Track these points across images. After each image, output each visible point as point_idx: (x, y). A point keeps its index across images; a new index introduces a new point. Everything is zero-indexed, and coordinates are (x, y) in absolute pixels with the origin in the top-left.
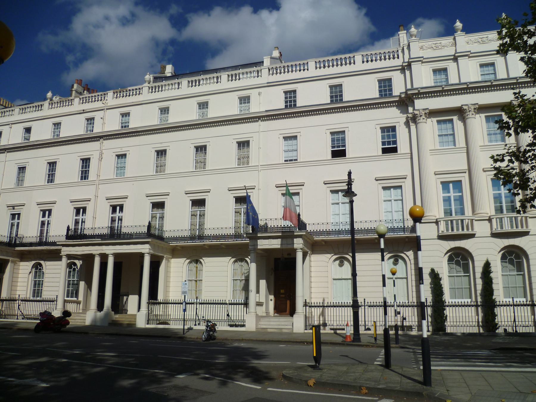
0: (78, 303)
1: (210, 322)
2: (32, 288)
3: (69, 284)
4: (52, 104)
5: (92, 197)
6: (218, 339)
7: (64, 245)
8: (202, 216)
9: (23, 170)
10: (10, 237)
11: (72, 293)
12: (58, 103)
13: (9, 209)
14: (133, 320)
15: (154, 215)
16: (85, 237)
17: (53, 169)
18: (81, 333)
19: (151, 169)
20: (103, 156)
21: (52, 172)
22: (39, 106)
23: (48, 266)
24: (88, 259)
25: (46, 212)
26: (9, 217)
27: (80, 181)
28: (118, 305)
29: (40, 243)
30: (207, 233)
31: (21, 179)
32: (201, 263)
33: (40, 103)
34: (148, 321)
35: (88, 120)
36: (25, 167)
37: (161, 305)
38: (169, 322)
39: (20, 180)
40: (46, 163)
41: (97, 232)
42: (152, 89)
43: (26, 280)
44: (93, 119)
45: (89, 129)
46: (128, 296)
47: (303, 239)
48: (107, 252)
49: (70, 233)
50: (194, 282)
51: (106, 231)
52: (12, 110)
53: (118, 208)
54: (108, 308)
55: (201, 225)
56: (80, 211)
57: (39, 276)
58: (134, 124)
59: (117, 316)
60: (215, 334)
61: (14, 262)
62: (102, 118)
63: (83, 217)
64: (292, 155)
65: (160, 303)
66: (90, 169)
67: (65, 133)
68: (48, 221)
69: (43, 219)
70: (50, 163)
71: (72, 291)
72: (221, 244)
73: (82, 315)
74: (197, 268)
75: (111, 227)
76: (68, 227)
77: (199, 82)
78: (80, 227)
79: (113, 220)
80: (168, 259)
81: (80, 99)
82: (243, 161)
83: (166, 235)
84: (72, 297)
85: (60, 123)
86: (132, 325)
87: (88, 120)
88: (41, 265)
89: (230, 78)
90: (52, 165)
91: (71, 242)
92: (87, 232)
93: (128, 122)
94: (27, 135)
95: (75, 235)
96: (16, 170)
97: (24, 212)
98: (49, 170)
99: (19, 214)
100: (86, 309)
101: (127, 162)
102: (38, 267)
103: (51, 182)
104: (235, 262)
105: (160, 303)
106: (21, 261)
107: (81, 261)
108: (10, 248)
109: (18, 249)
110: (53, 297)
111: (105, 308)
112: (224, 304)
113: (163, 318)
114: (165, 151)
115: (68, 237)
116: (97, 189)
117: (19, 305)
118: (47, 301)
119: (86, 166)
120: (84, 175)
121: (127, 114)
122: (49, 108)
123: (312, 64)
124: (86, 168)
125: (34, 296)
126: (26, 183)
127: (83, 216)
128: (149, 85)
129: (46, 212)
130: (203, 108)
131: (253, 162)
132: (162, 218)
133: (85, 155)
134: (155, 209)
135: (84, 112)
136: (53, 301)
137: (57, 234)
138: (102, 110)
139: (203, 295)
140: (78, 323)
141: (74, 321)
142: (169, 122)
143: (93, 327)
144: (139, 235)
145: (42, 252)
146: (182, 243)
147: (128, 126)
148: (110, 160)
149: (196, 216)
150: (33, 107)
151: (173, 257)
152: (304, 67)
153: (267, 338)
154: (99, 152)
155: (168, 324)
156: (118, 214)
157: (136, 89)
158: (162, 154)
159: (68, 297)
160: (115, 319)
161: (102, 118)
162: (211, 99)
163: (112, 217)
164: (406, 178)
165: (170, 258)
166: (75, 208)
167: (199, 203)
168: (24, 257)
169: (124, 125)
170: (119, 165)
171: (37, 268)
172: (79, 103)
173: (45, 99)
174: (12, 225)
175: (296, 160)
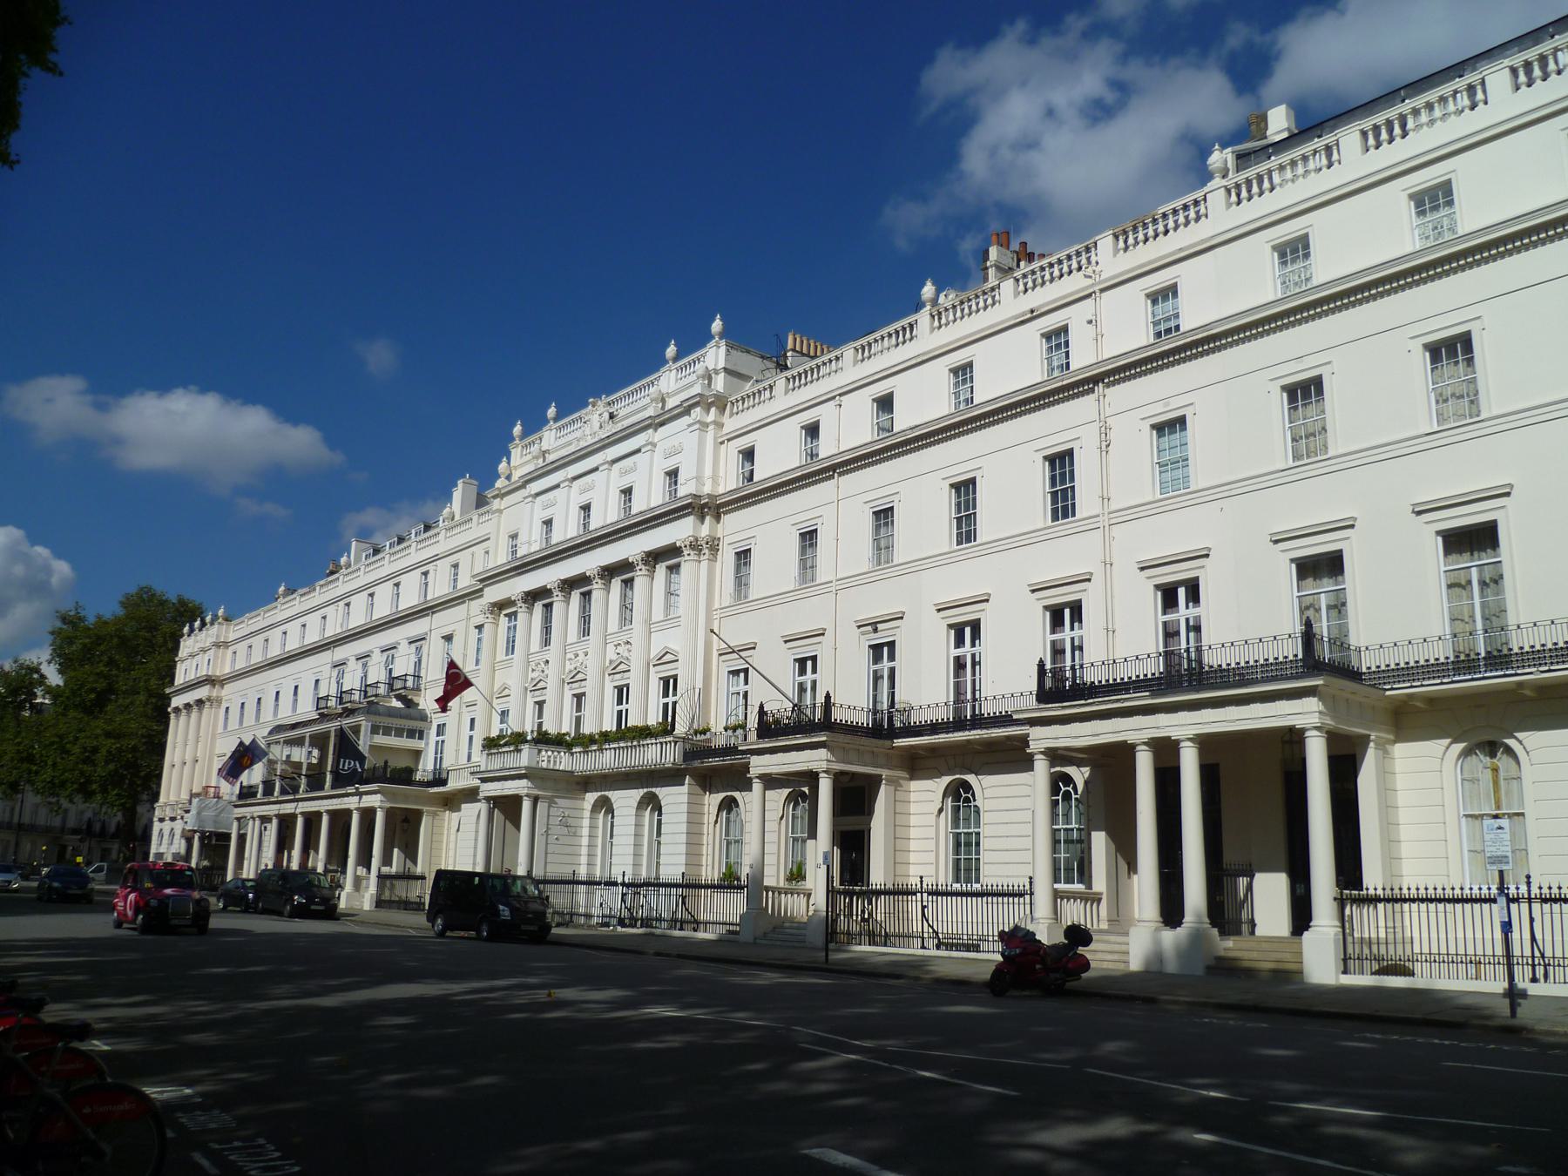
2: (951, 857)
4: (940, 314)
5: (1095, 568)
7: (1033, 722)
8: (1494, 582)
10: (875, 712)
11: (1069, 870)
12: (954, 307)
13: (863, 634)
14: (1288, 957)
16: (1092, 691)
18: (1131, 999)
19: (1278, 452)
20: (1112, 435)
21: (967, 509)
22: (904, 329)
23: (990, 789)
24: (1113, 763)
25: (966, 631)
26: (865, 655)
27: (1049, 523)
28: (1227, 911)
29: (959, 724)
30: (1520, 641)
31: (883, 545)
32: (1509, 751)
33: (905, 322)
34: (1345, 960)
35: (1048, 336)
36: (892, 508)
37: (1381, 906)
39: (882, 548)
41: (1125, 673)
42: (1238, 194)
44: (1064, 329)
45: (1055, 364)
46: (1252, 877)
48: (1174, 734)
51: (1154, 668)
52: (837, 359)
53: (1182, 592)
54: (1199, 916)
55: (1495, 617)
56: (1063, 614)
57: (967, 819)
58: (1194, 315)
59: (1230, 943)
62: (1090, 322)
63: (1073, 634)
65: (1375, 900)
66: (1076, 484)
67: (989, 388)
68: (973, 656)
69: (959, 652)
70: (956, 487)
71: (1072, 864)
73: (1113, 938)
74: (1495, 770)
76: (1041, 665)
77: (1403, 126)
78: (1068, 663)
79: (1170, 634)
80: (1382, 747)
81: (1017, 280)
82: (1308, 443)
83: (1367, 662)
84: (1069, 880)
85: (970, 365)
86: (1288, 976)
87: (1048, 336)
88: (967, 787)
89: (1522, 78)
90: (965, 489)
91: (1055, 710)
92: (1091, 676)
93: (1177, 316)
95: (1060, 688)
96: (868, 521)
97: (902, 636)
98: (958, 505)
99: (891, 645)
101: (1189, 440)
102: (960, 794)
105: (1375, 900)
106: (912, 778)
107: (1086, 771)
111: (1189, 917)
113: (1394, 953)
114: (1317, 382)
115: (1044, 696)
116: (1107, 542)
117: (923, 908)
118: (993, 894)
119: (1063, 475)
120: (1063, 504)
121: (1171, 291)
122: (932, 329)
123: (1105, 242)
124: (1063, 482)
127: (1072, 629)
128: (1224, 182)
129: (966, 631)
130: (1435, 208)
131: (1493, 401)
132: (1339, 607)
133: (805, 521)
134: (1310, 581)
135: (1034, 315)
136: (1021, 895)
137: (1007, 691)
138: (1089, 296)
139: (977, 870)
140: (1105, 965)
141: (1101, 957)
142: (1315, 282)
143: (1154, 973)
144: (1274, 671)
145: (972, 749)
146: (1432, 687)
147: (1177, 328)
148: (1136, 447)
150: (890, 335)
152: (1195, 211)
154: (1096, 425)
155: (1410, 973)
156: (1183, 612)
157: (1175, 212)
158: (1307, 395)
160: (1222, 953)
161: (1090, 322)
162: (1460, 170)
163: (1165, 624)
166: (1157, 587)
167: (1474, 539)
168: (918, 765)
169: (1162, 328)
170: (1166, 457)
171: (957, 798)
172: (1017, 294)
173: (918, 306)
174: (877, 677)
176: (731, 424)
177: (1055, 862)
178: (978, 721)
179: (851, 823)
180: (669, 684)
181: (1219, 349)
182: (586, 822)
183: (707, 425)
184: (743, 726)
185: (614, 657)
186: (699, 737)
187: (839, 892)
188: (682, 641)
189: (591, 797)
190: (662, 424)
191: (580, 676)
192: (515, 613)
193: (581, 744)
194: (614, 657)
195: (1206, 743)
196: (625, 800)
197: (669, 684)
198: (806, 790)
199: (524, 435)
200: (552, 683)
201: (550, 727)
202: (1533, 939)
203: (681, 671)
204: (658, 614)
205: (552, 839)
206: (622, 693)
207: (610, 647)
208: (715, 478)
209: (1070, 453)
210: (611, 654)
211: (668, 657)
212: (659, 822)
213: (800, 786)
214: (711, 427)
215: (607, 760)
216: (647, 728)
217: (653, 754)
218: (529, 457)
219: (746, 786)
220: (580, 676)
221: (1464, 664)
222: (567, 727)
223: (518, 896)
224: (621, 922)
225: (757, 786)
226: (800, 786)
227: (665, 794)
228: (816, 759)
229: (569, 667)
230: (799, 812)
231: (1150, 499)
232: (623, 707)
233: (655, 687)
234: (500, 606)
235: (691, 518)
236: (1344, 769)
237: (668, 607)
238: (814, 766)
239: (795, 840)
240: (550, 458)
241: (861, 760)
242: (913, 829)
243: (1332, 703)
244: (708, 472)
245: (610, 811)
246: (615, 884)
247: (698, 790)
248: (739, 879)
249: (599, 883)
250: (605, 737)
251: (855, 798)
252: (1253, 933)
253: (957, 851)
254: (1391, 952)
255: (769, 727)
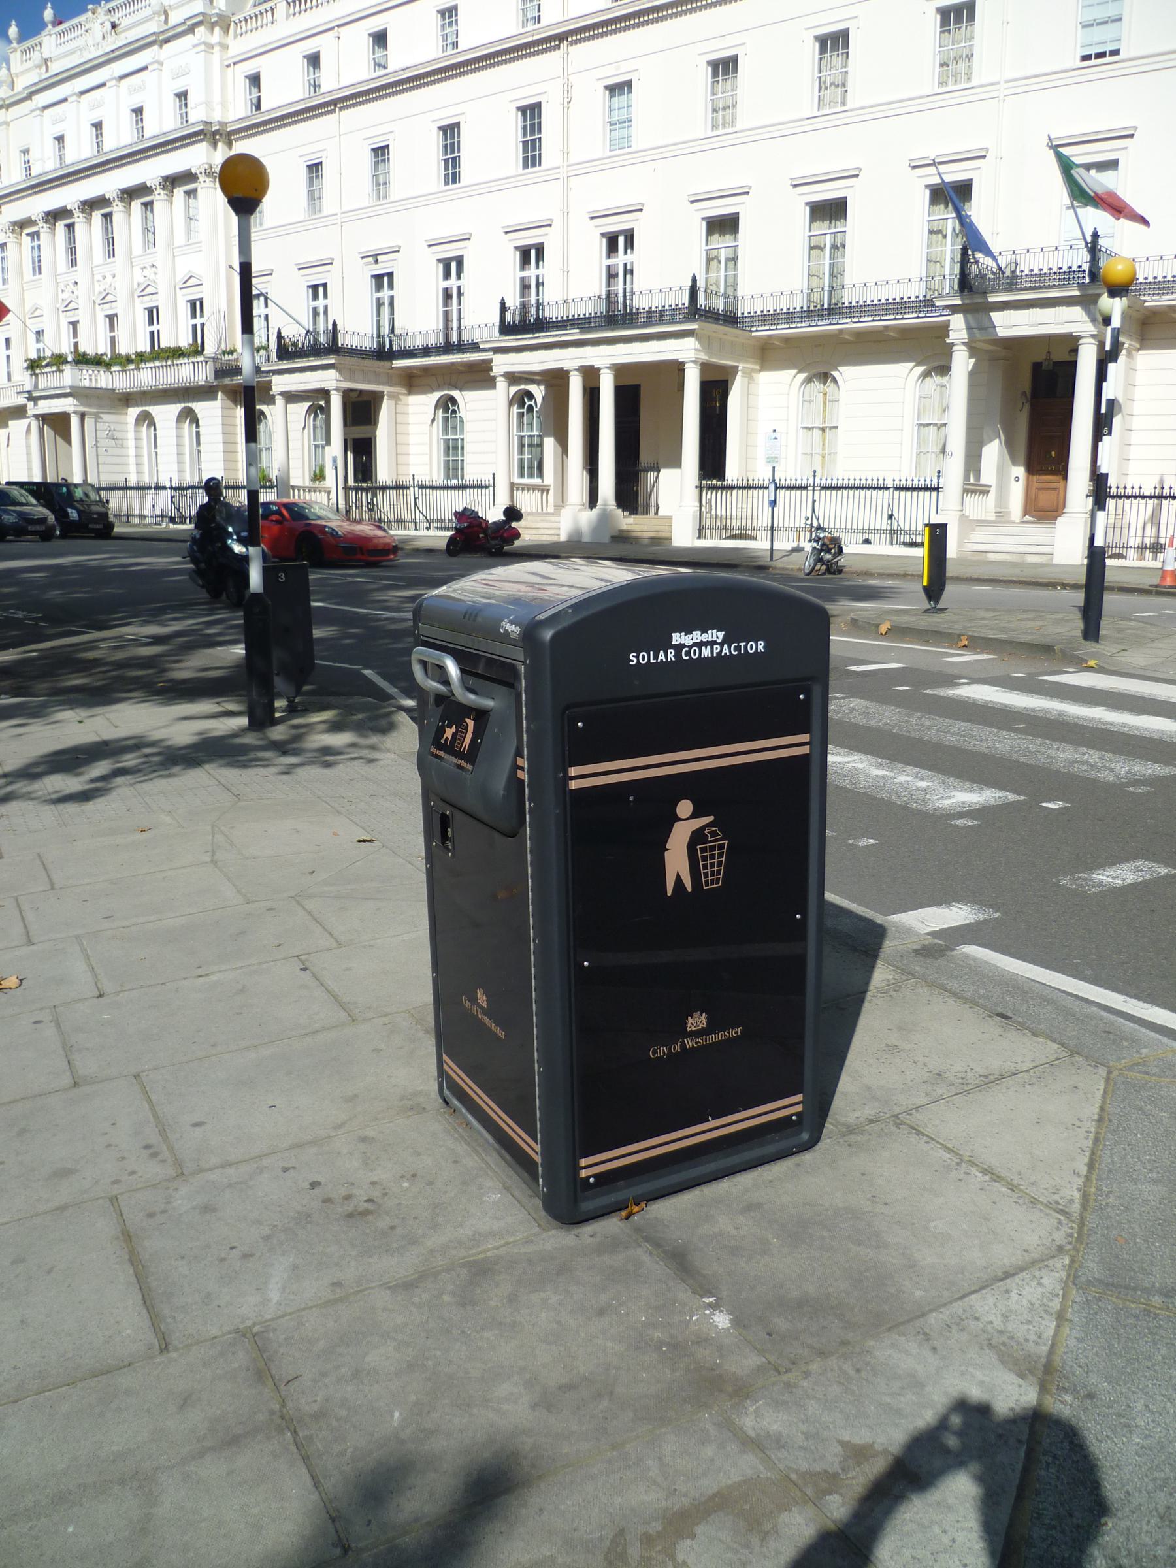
0: (545, 490)
1: (824, 530)
3: (522, 446)
6: (847, 573)
7: (497, 350)
9: (383, 154)
10: (379, 336)
11: (531, 468)
13: (367, 264)
15: (714, 253)
17: (532, 126)
20: (574, 93)
21: (532, 133)
23: (469, 401)
24: (556, 380)
25: (452, 266)
26: (369, 284)
28: (630, 494)
29: (448, 347)
30: (850, 297)
32: (834, 380)
34: (700, 530)
36: (388, 146)
37: (735, 492)
38: (754, 533)
40: (515, 110)
41: (575, 311)
43: (426, 438)
46: (658, 472)
47: (699, 339)
49: (509, 317)
50: (818, 432)
53: (621, 240)
56: (529, 254)
57: (454, 428)
59: (632, 519)
60: (842, 561)
61: (395, 397)
64: (1101, 39)
65: (732, 488)
66: (543, 135)
68: (459, 288)
69: (447, 284)
70: (523, 110)
72: (886, 327)
73: (553, 518)
75: (608, 294)
79: (611, 275)
80: (749, 374)
83: (744, 309)
84: (531, 476)
88: (453, 401)
94: (380, 53)
95: (523, 324)
96: (368, 156)
97: (470, 253)
100: (561, 503)
101: (634, 103)
102: (448, 405)
103: (454, 182)
104: (926, 375)
105: (732, 488)
106: (410, 393)
107: (542, 388)
108: (382, 363)
109: (397, 363)
110: (486, 478)
112: (880, 488)
114: (844, 35)
115: (506, 329)
118: (473, 487)
120: (531, 154)
125: (448, 477)
126: (745, 117)
129: (452, 266)
136: (486, 487)
145: (452, 370)
146: (783, 330)
149: (822, 249)
151: (763, 369)
153: (1027, 574)
154: (560, 82)
155: (751, 538)
159: (522, 475)
160: (625, 527)
164: (1132, 136)
165: (753, 370)
166: (516, 248)
167: (831, 211)
168: (413, 382)
170: (615, 119)
171: (446, 409)
174: (379, 304)
175: (1116, 52)
176: (238, 45)
177: (521, 461)
178: (461, 347)
179: (360, 432)
180: (196, 307)
181: (662, 19)
182: (131, 435)
183: (211, 46)
184: (266, 348)
185: (142, 280)
186: (227, 357)
187: (350, 488)
188: (120, 277)
189: (133, 412)
190: (167, 41)
191: (109, 298)
192: (37, 233)
193: (120, 364)
194: (142, 280)
195: (620, 370)
196: (166, 414)
197: (196, 307)
198: (322, 403)
199: (22, 38)
200: (83, 304)
201: (86, 348)
202: (814, 511)
203: (205, 293)
204: (180, 238)
205: (101, 451)
206: (152, 315)
207: (137, 270)
208: (224, 103)
209: (458, 125)
210: (138, 277)
211: (192, 282)
212: (198, 433)
213: (317, 400)
214: (217, 49)
215: (144, 378)
216: (179, 349)
217: (186, 373)
218: (30, 64)
219: (271, 400)
220: (109, 298)
221: (812, 314)
222: (102, 348)
223: (81, 500)
224: (173, 520)
225: (279, 401)
226: (317, 400)
227: (201, 408)
228: (328, 379)
229: (98, 289)
230: (318, 422)
231: (600, 156)
232: (155, 328)
233: (184, 310)
234: (21, 225)
235: (204, 144)
236: (715, 393)
237: (188, 231)
238: (325, 385)
239: (317, 446)
240: (55, 68)
241: (367, 382)
242: (409, 434)
243: (707, 343)
244: (217, 97)
245: (152, 424)
246: (164, 488)
247: (230, 404)
248: (270, 481)
249: (150, 488)
250: (141, 357)
251: (362, 410)
252: (657, 513)
253: (447, 454)
254: (739, 524)
255: (286, 351)
